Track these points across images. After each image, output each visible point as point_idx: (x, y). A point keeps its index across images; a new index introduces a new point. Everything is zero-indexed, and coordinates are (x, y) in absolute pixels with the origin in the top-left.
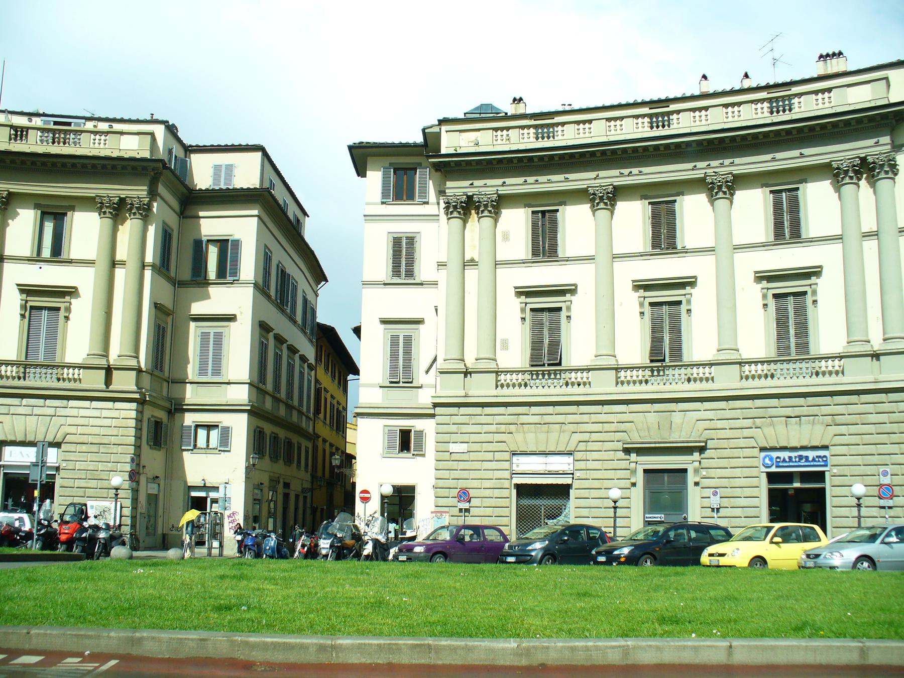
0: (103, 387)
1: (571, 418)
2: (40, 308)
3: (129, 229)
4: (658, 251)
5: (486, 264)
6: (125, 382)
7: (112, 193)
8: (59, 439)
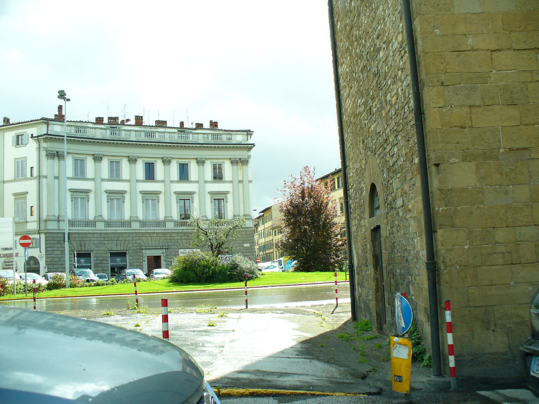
5: (51, 177)
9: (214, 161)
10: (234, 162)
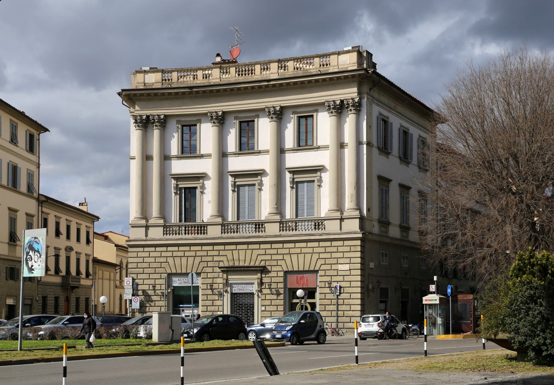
0: (144, 238)
2: (303, 182)
3: (350, 120)
6: (353, 226)
7: (270, 105)
8: (317, 269)
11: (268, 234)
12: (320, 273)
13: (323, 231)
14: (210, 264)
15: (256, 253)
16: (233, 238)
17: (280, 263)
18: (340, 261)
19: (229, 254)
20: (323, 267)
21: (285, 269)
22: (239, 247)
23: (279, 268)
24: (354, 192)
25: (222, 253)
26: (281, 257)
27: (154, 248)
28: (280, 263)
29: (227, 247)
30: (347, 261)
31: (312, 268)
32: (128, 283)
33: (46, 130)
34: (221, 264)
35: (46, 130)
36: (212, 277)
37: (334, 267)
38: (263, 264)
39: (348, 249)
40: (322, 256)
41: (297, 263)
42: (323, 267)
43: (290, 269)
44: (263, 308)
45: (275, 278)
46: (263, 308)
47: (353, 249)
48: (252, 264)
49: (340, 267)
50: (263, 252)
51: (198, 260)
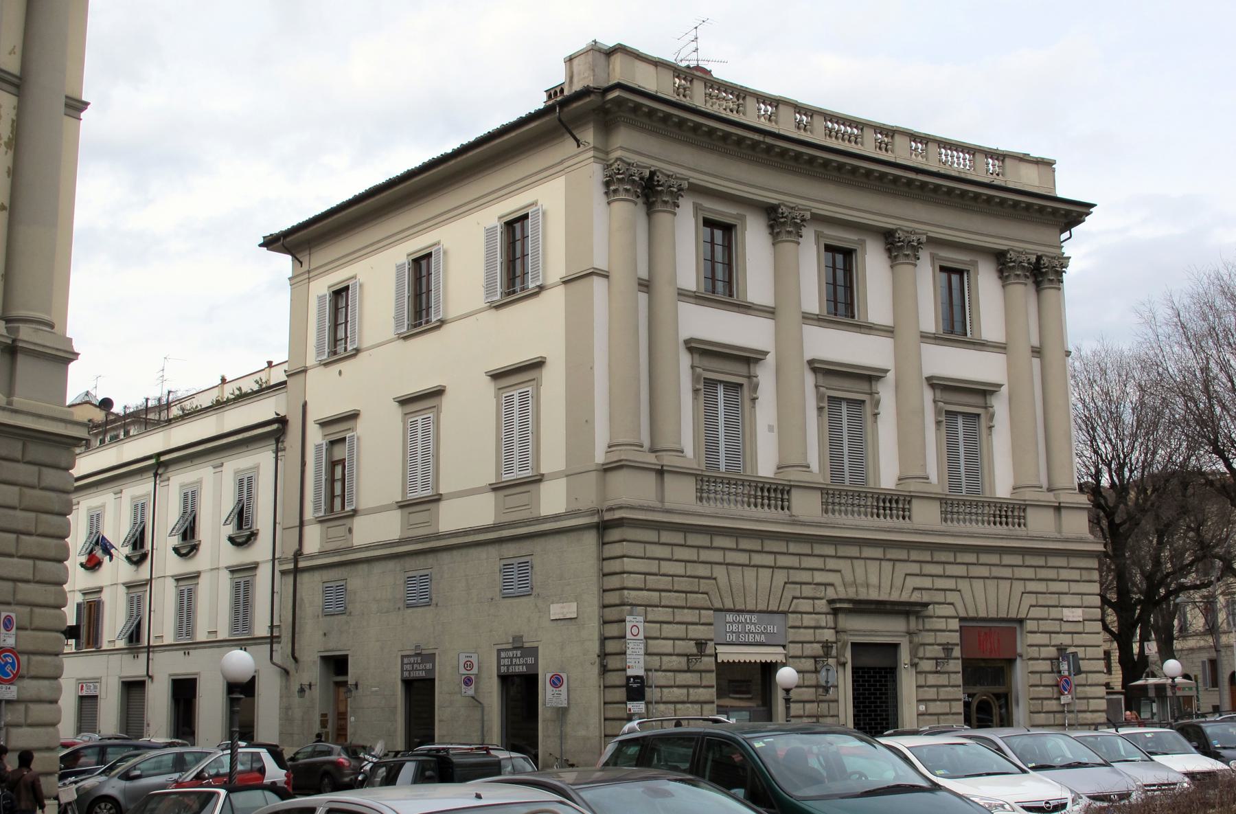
1: (783, 561)
4: (833, 318)
8: (1022, 615)
9: (708, 204)
10: (1003, 262)
11: (916, 526)
12: (1030, 625)
13: (900, 523)
14: (808, 591)
15: (902, 568)
16: (901, 531)
17: (951, 597)
18: (1066, 600)
19: (843, 565)
20: (1035, 612)
21: (962, 614)
22: (868, 552)
23: (949, 611)
24: (50, 423)
25: (832, 564)
26: (950, 584)
27: (681, 535)
28: (951, 597)
29: (843, 550)
30: (1076, 600)
31: (1013, 615)
32: (635, 631)
33: (1093, 206)
34: (831, 593)
35: (1093, 206)
36: (813, 624)
37: (1054, 613)
38: (916, 597)
39: (1075, 575)
40: (1032, 586)
41: (986, 598)
42: (1035, 612)
43: (972, 614)
44: (922, 708)
45: (944, 628)
46: (922, 708)
47: (1086, 575)
48: (895, 597)
49: (1068, 614)
50: (915, 568)
51: (781, 577)
